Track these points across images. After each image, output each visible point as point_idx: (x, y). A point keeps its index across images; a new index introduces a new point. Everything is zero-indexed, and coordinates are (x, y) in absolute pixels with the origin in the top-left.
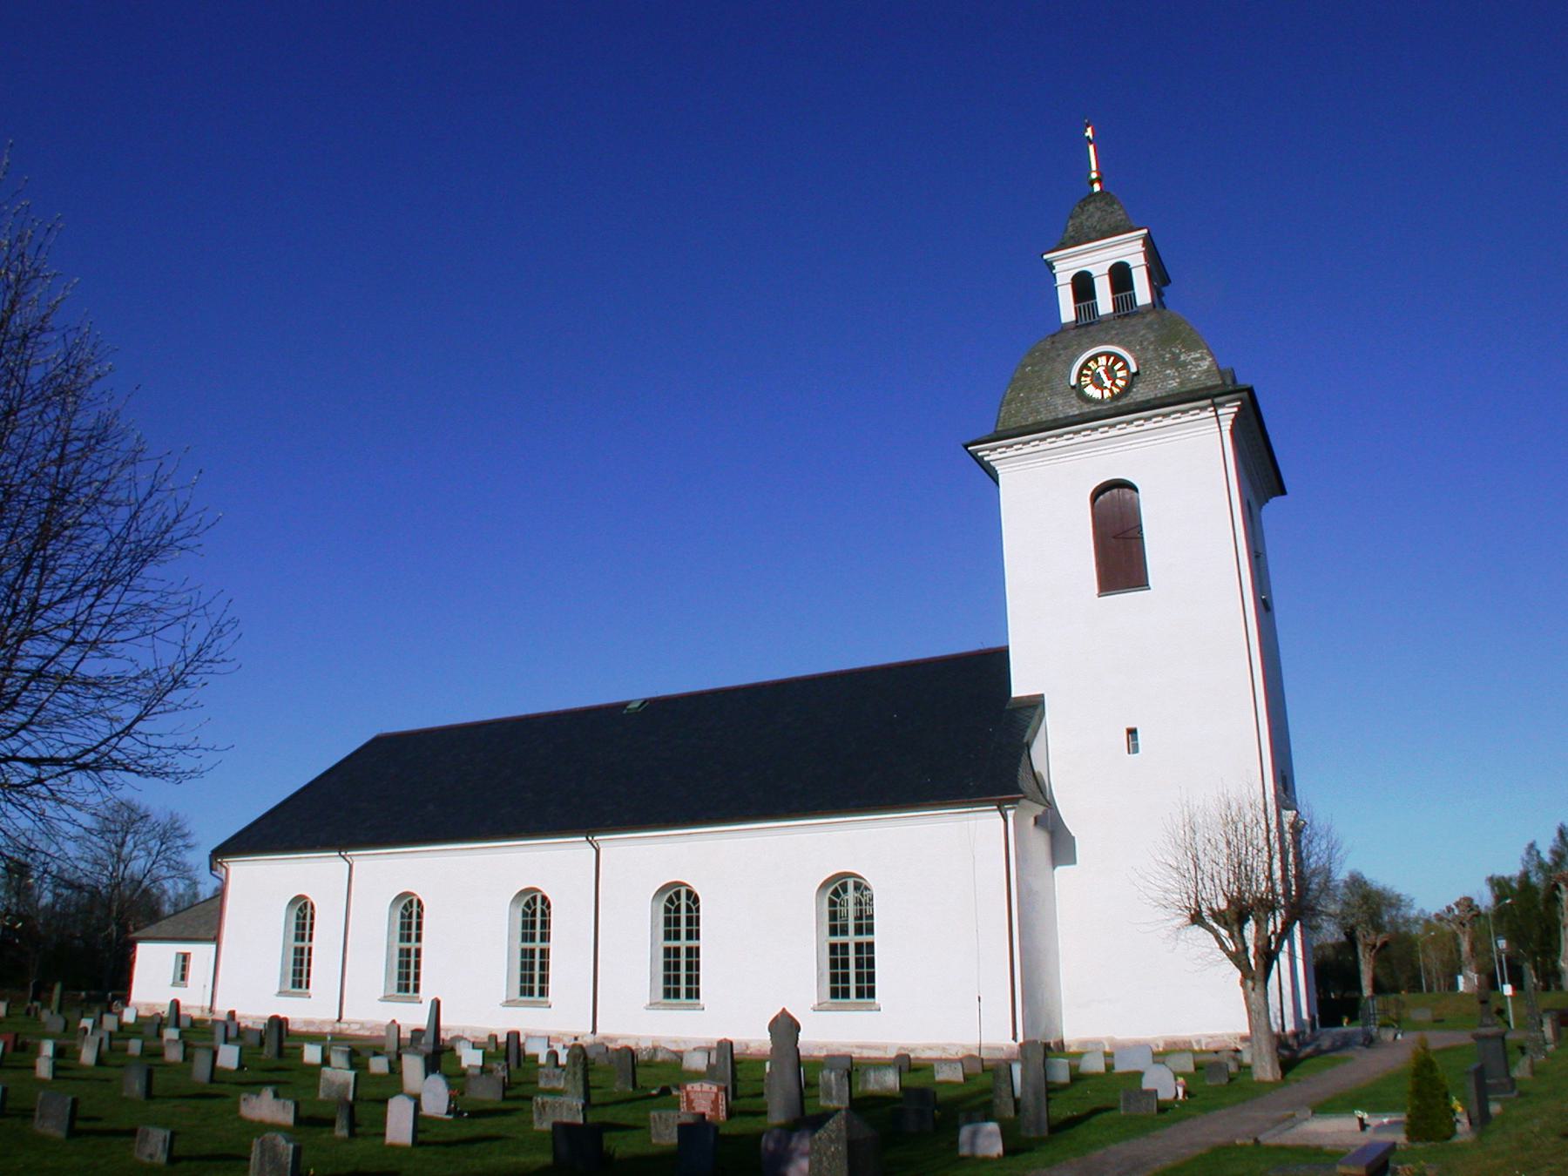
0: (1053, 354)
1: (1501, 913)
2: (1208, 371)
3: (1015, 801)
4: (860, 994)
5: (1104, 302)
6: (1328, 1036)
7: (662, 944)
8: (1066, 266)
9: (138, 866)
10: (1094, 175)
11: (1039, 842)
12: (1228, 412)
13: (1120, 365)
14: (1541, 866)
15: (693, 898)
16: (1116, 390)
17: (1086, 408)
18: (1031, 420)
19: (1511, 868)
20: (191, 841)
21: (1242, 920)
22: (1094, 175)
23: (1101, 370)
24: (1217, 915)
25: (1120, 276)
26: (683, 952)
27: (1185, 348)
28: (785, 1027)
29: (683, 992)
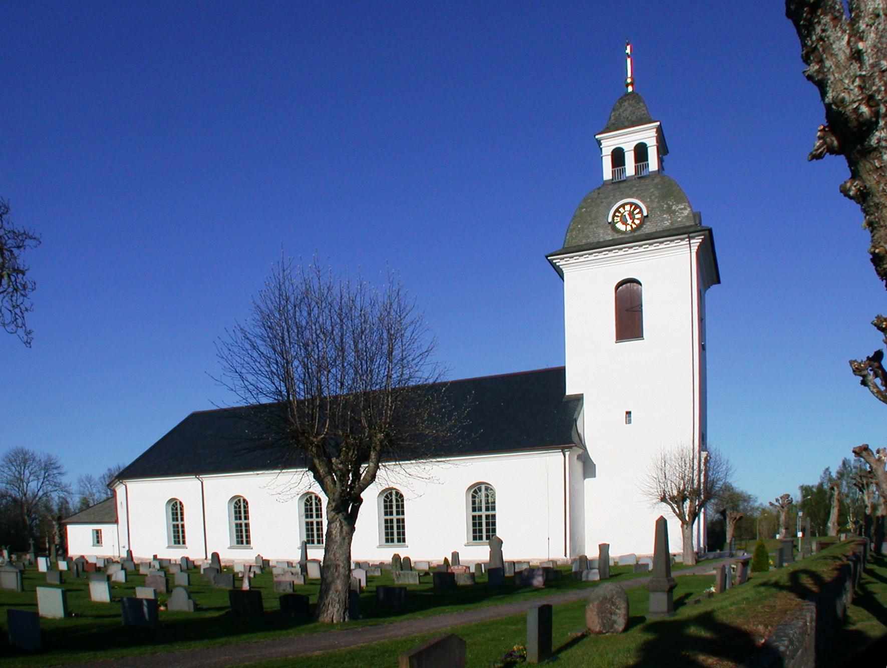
0: (598, 201)
1: (804, 505)
2: (687, 216)
3: (571, 447)
5: (630, 168)
6: (711, 555)
7: (383, 517)
8: (609, 143)
9: (33, 485)
10: (629, 81)
11: (579, 466)
12: (696, 242)
13: (638, 210)
14: (831, 479)
15: (400, 496)
16: (634, 226)
17: (616, 236)
18: (584, 242)
19: (813, 481)
20: (63, 471)
21: (684, 499)
22: (629, 81)
23: (626, 214)
24: (673, 498)
25: (641, 152)
27: (677, 206)
28: (455, 555)
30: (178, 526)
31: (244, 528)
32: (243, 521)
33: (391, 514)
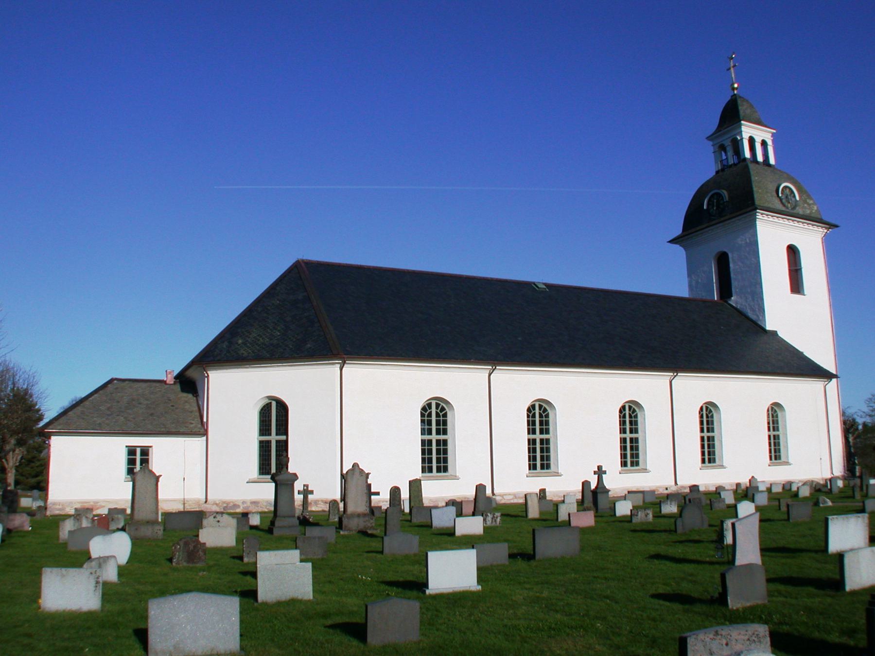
4: (542, 467)
15: (283, 408)
26: (538, 441)
29: (538, 466)
30: (708, 431)
31: (628, 426)
32: (628, 436)
33: (438, 442)
